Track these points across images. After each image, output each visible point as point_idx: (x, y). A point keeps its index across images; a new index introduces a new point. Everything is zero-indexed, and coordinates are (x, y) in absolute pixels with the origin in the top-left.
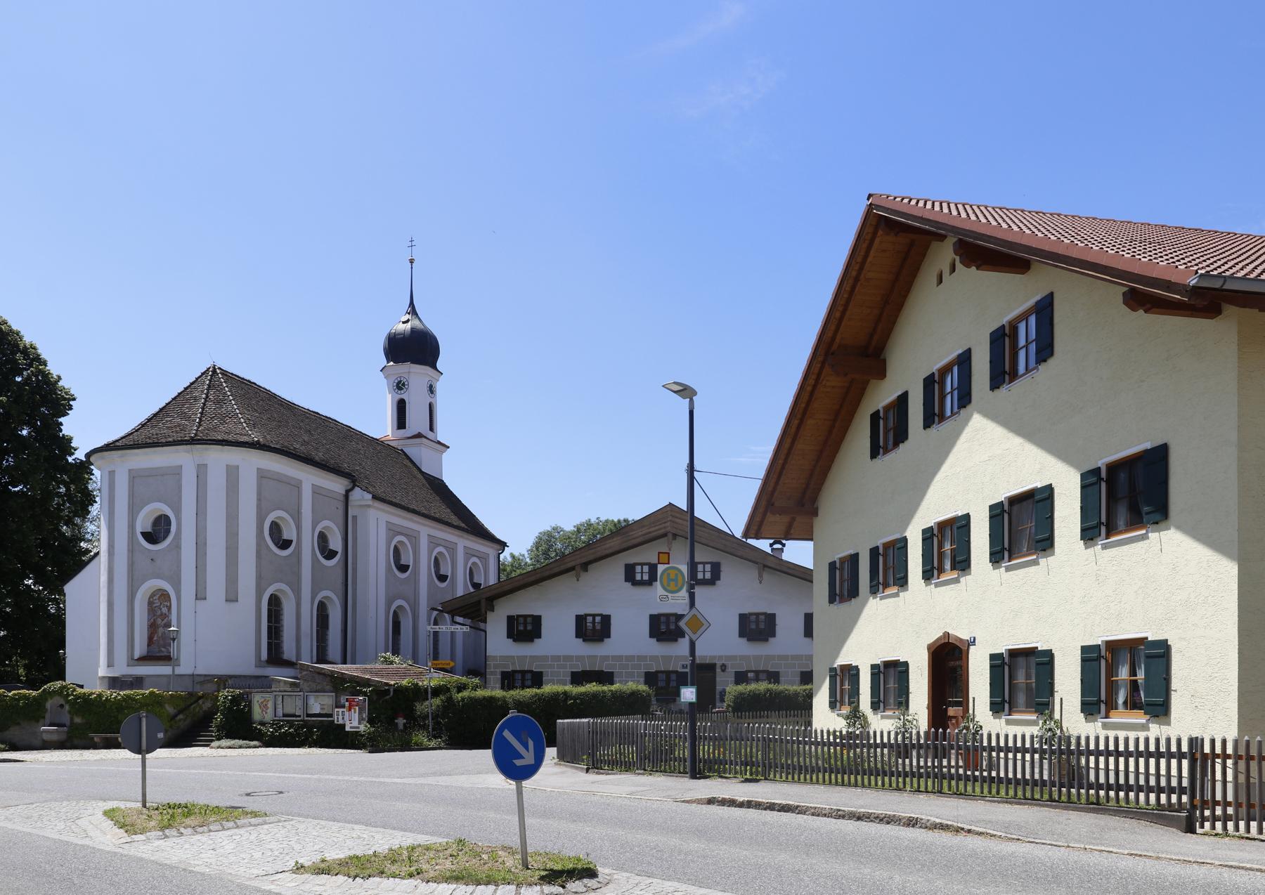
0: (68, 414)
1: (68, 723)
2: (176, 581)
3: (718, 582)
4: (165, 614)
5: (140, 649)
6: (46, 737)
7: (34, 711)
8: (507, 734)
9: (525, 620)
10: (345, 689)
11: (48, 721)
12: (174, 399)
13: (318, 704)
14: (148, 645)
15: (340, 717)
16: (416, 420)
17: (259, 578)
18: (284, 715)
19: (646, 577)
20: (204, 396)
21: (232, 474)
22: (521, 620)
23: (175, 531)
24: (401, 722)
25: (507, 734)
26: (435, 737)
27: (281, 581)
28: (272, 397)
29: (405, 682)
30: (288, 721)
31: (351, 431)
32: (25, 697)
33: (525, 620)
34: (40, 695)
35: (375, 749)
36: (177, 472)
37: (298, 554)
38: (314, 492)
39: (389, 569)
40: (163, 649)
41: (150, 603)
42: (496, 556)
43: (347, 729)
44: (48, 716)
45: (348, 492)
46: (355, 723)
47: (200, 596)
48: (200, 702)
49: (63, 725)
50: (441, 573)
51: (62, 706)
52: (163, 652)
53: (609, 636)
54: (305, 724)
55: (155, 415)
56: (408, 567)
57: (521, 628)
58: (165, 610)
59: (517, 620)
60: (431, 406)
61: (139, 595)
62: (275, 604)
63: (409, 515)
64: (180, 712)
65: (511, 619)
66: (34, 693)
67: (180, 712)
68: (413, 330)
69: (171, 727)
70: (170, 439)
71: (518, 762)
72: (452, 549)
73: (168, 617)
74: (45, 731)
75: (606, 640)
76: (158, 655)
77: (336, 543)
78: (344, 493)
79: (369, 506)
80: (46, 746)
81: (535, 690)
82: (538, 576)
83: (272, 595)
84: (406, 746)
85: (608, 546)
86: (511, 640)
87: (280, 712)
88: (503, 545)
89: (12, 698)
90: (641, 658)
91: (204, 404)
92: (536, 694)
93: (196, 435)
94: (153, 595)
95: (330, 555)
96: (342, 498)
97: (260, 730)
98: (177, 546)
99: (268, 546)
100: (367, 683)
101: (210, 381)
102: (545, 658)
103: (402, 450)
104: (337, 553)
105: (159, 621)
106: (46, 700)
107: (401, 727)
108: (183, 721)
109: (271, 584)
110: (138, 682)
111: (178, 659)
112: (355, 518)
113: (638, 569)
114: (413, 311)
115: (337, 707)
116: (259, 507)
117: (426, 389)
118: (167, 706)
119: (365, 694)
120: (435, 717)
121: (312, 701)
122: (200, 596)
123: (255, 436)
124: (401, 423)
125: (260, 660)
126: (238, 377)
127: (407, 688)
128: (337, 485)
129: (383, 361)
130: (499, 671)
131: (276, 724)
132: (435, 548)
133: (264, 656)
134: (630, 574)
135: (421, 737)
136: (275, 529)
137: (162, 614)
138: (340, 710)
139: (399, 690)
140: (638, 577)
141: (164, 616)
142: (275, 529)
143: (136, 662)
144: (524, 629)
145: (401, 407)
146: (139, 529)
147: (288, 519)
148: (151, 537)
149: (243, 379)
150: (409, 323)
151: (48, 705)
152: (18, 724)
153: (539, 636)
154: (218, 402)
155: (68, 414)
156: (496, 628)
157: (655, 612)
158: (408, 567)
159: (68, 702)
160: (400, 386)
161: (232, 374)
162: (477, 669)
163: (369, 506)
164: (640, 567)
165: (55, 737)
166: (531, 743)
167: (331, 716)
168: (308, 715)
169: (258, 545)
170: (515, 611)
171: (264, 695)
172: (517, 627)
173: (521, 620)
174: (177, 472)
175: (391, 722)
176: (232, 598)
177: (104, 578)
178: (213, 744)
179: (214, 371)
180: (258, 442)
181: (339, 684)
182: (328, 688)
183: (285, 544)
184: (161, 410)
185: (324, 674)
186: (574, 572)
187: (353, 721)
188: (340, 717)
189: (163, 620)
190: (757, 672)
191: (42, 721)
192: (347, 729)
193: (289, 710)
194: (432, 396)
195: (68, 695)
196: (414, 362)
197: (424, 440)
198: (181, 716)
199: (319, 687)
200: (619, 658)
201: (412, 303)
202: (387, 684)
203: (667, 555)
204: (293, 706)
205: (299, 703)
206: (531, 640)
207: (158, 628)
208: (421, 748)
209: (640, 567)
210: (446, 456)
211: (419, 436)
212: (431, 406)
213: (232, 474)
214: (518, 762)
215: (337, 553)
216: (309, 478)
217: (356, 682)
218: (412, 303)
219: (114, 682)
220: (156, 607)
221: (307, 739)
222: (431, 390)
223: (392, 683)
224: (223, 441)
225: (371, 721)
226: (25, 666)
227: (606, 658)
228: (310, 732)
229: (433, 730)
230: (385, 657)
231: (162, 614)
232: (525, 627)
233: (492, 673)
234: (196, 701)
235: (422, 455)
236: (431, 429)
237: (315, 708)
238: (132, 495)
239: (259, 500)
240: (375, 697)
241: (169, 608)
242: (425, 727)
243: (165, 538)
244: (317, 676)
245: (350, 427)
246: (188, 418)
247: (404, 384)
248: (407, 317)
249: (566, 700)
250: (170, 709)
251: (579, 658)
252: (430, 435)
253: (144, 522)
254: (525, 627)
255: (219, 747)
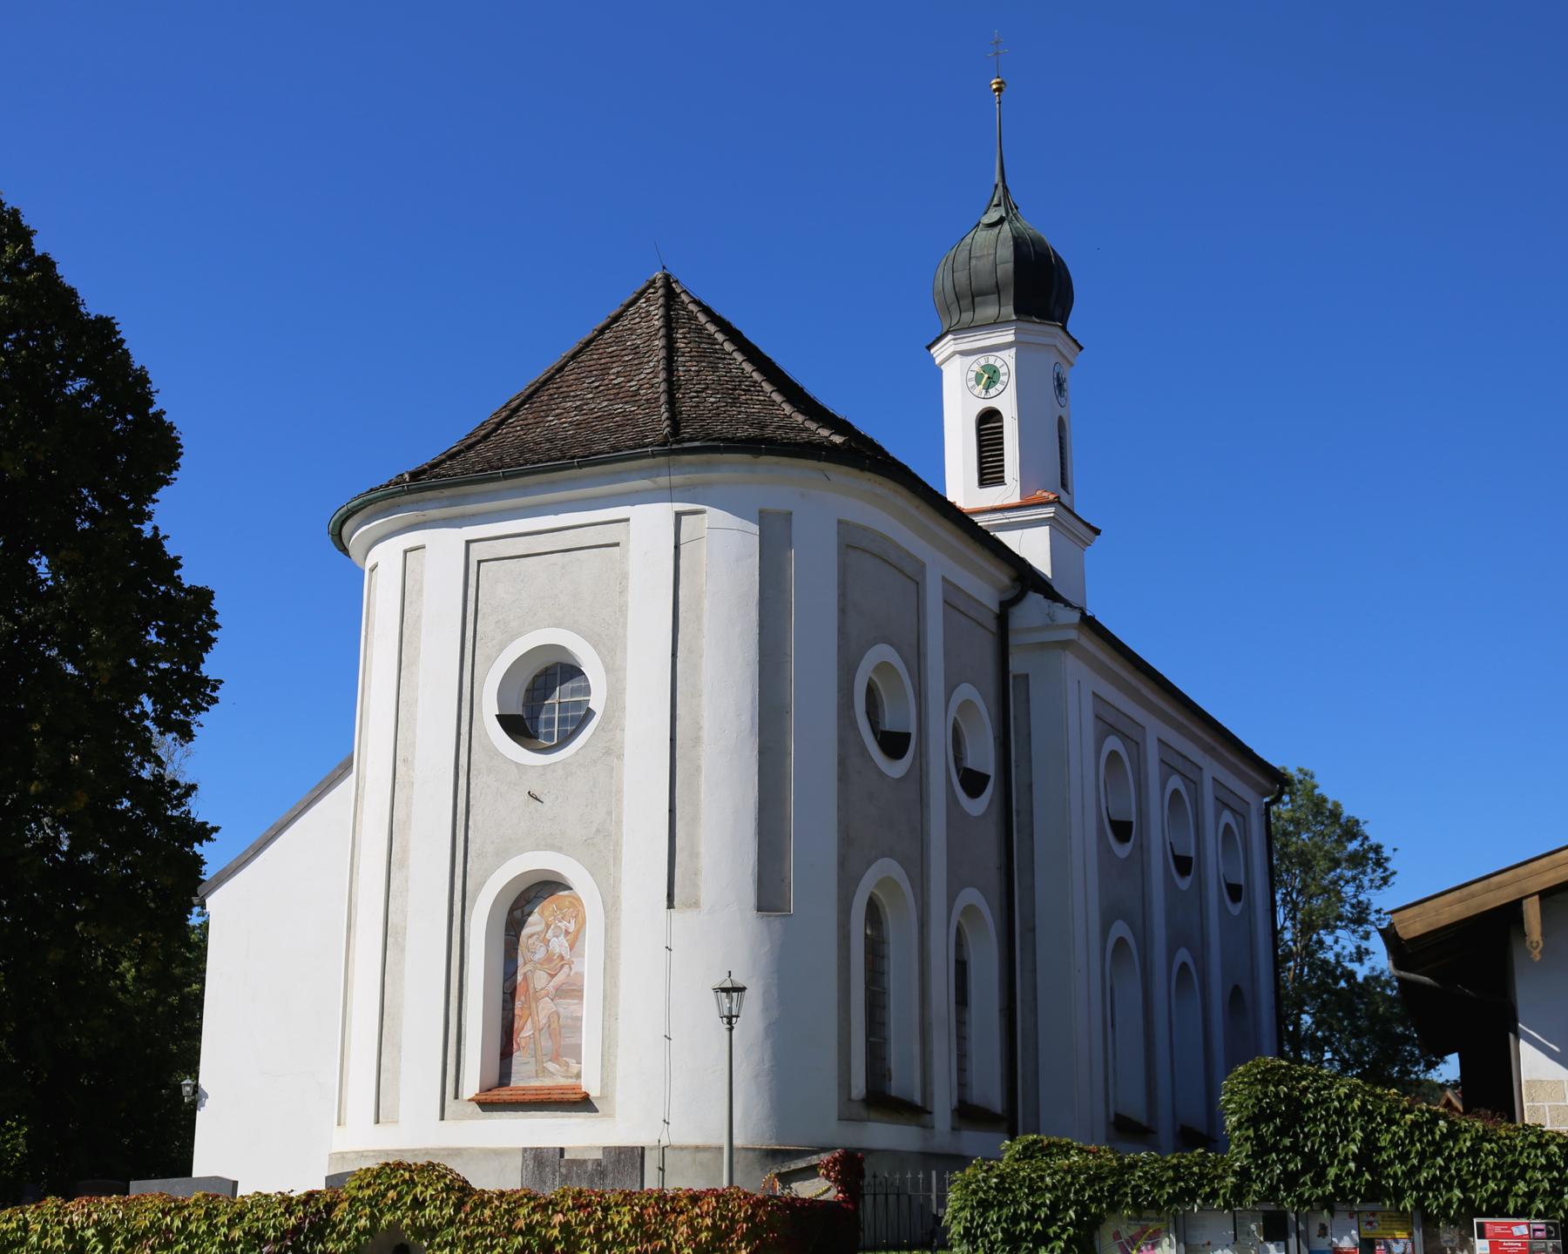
0: (214, 640)
4: (562, 958)
23: (1133, 941)
40: (551, 1066)
45: (1006, 607)
50: (887, 728)
52: (552, 1074)
56: (906, 737)
58: (559, 945)
60: (1061, 423)
73: (570, 964)
76: (535, 1083)
78: (995, 608)
96: (992, 624)
99: (864, 750)
109: (869, 864)
125: (850, 1099)
133: (859, 1087)
137: (549, 959)
147: (901, 672)
150: (1006, 226)
155: (214, 640)
158: (906, 737)
169: (842, 742)
189: (553, 976)
203: (472, 546)
207: (537, 1000)
220: (531, 936)
231: (549, 959)
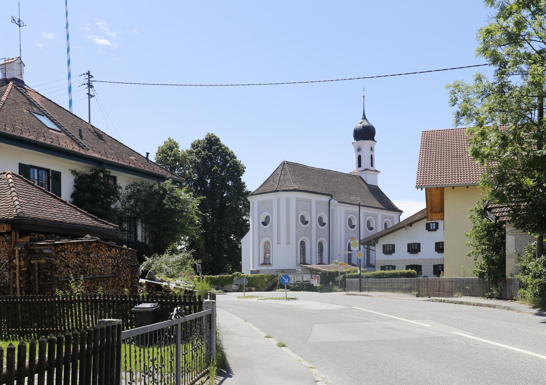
1: (239, 284)
2: (272, 238)
3: (437, 230)
5: (262, 261)
6: (234, 289)
7: (230, 281)
8: (283, 277)
9: (389, 246)
10: (314, 273)
11: (234, 284)
12: (271, 175)
13: (306, 278)
14: (264, 260)
15: (312, 282)
16: (366, 163)
17: (297, 235)
18: (297, 281)
19: (434, 228)
20: (280, 173)
21: (288, 200)
22: (413, 245)
24: (331, 283)
25: (283, 277)
26: (341, 288)
27: (305, 236)
28: (304, 167)
29: (333, 271)
30: (298, 283)
31: (336, 173)
32: (228, 277)
33: (389, 246)
34: (232, 276)
35: (321, 292)
36: (271, 201)
37: (311, 226)
38: (317, 203)
39: (346, 227)
41: (265, 246)
42: (398, 217)
43: (314, 285)
44: (234, 282)
45: (330, 201)
46: (316, 284)
47: (278, 243)
48: (276, 278)
49: (238, 285)
51: (238, 279)
53: (394, 252)
54: (302, 284)
55: (266, 181)
57: (413, 248)
58: (269, 248)
59: (386, 246)
60: (371, 156)
61: (261, 243)
62: (303, 244)
63: (352, 206)
64: (269, 281)
65: (384, 246)
66: (231, 276)
67: (269, 281)
68: (364, 127)
69: (266, 285)
70: (269, 191)
71: (285, 282)
72: (376, 217)
74: (233, 287)
75: (419, 253)
77: (325, 220)
79: (337, 205)
80: (234, 291)
81: (372, 273)
82: (392, 230)
83: (301, 241)
84: (331, 291)
85: (416, 217)
86: (384, 254)
87: (295, 281)
88: (401, 212)
89: (225, 277)
90: (432, 259)
91: (280, 176)
92: (374, 274)
93: (277, 189)
94: (265, 243)
95: (323, 224)
96: (328, 203)
97: (290, 286)
98: (272, 226)
99: (300, 224)
100: (320, 271)
101: (282, 167)
102: (396, 260)
103: (360, 176)
104: (326, 223)
105: (267, 251)
106: (234, 277)
107: (331, 285)
108: (270, 284)
110: (258, 272)
111: (272, 264)
112: (332, 210)
113: (431, 224)
114: (364, 118)
115: (311, 278)
116: (297, 211)
117: (369, 149)
118: (265, 279)
119: (319, 274)
120: (341, 282)
121: (304, 277)
122: (278, 243)
123: (295, 186)
124: (360, 165)
126: (292, 163)
127: (333, 272)
128: (326, 199)
129: (353, 140)
130: (380, 266)
131: (294, 284)
132: (367, 218)
134: (428, 228)
135: (336, 288)
136: (303, 218)
138: (312, 280)
139: (330, 273)
140: (431, 228)
141: (269, 250)
142: (303, 218)
143: (261, 266)
144: (389, 250)
145: (359, 158)
146: (261, 221)
148: (265, 224)
149: (294, 163)
151: (234, 279)
152: (227, 285)
153: (420, 251)
154: (285, 175)
156: (379, 248)
157: (438, 241)
159: (239, 278)
160: (359, 150)
161: (290, 162)
162: (369, 265)
163: (337, 205)
164: (432, 224)
165: (236, 289)
166: (287, 279)
167: (310, 281)
168: (303, 281)
169: (297, 224)
170: (385, 243)
171: (291, 275)
172: (411, 248)
173: (413, 245)
174: (271, 201)
175: (327, 283)
176: (288, 243)
177: (251, 238)
178: (277, 290)
179: (284, 163)
180: (296, 189)
181: (312, 271)
182: (309, 272)
183: (306, 223)
184: (267, 179)
185: (308, 268)
186: (404, 228)
187: (316, 283)
188: (312, 282)
190: (389, 266)
191: (233, 284)
192: (314, 285)
193: (298, 280)
194: (372, 152)
195: (239, 276)
196: (364, 139)
197: (368, 171)
198: (269, 282)
199: (306, 272)
200: (424, 260)
201: (364, 115)
202: (326, 271)
204: (299, 279)
205: (301, 278)
206: (391, 254)
208: (335, 291)
209: (432, 224)
210: (379, 176)
211: (366, 170)
212: (371, 156)
213: (288, 200)
214: (285, 282)
215: (326, 223)
216: (314, 198)
217: (317, 271)
218: (364, 115)
219: (252, 272)
221: (303, 289)
222: (372, 149)
223: (328, 271)
224: (285, 190)
225: (321, 283)
226: (231, 267)
227: (419, 260)
228: (304, 287)
229: (340, 286)
230: (335, 262)
232: (415, 248)
233: (377, 267)
234: (274, 277)
235: (369, 179)
236: (372, 165)
237: (305, 279)
238: (259, 210)
239: (297, 209)
240: (322, 276)
241: (270, 247)
242: (337, 285)
243: (268, 223)
244: (306, 269)
245: (336, 172)
246: (275, 182)
247: (360, 149)
248: (362, 120)
249: (383, 275)
250: (266, 280)
251: (409, 260)
252: (371, 168)
253: (263, 219)
254: (415, 248)
255: (278, 291)
